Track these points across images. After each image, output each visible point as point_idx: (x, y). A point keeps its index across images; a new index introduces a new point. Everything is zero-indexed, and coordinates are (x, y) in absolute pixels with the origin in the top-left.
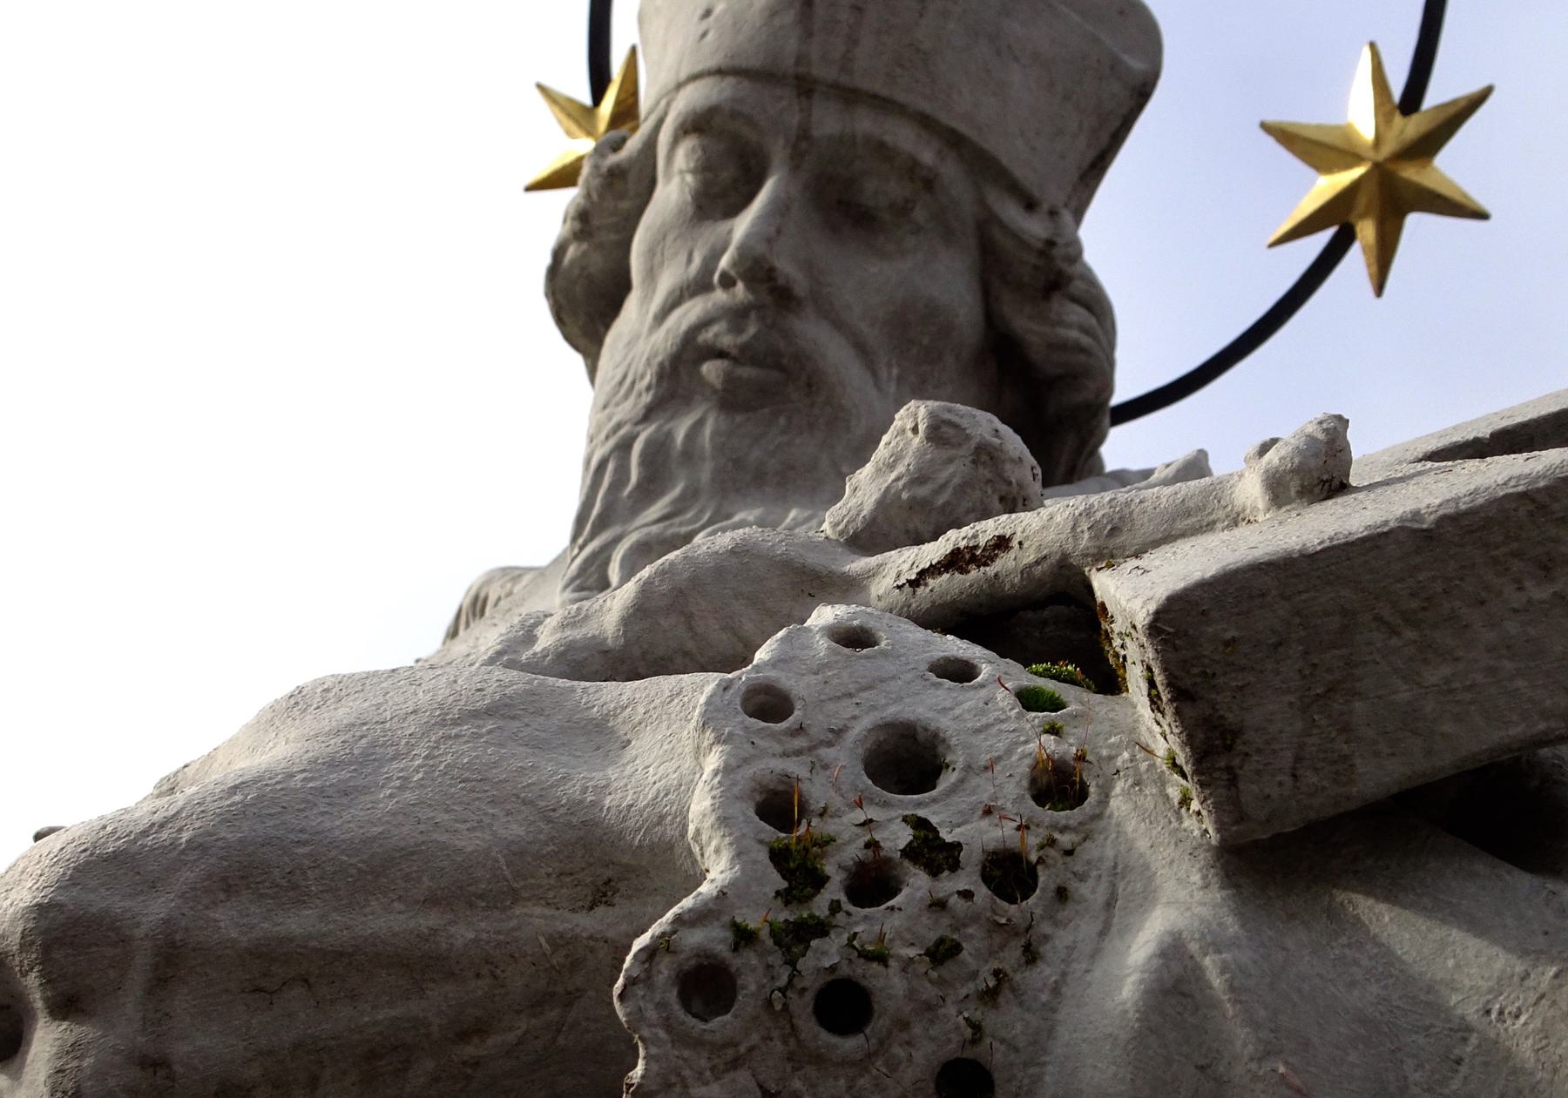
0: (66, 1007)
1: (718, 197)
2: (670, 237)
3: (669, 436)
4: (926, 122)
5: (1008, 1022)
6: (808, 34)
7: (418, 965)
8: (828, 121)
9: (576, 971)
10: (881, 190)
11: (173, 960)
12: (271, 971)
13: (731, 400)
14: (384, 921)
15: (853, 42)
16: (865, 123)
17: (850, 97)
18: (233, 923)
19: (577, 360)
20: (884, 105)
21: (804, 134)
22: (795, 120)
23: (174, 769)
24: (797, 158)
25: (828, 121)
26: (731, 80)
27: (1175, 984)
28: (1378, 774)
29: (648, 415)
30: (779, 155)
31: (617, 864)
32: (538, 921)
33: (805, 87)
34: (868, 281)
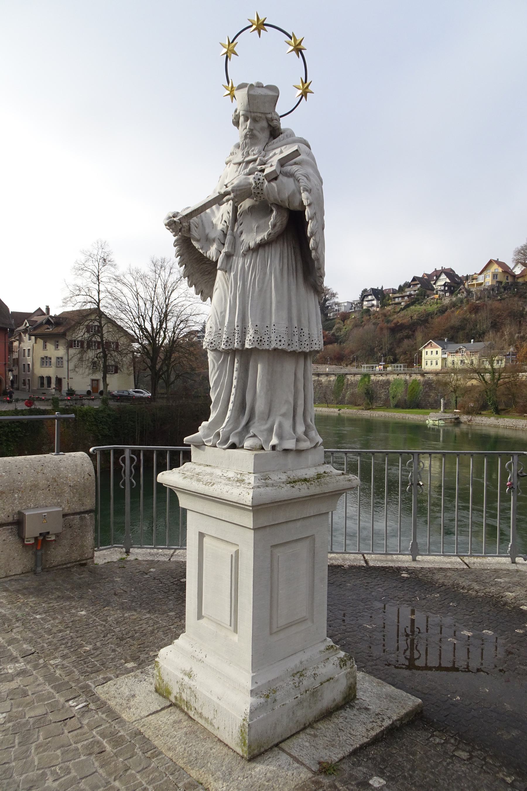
0: (233, 192)
1: (246, 120)
4: (260, 113)
7: (245, 189)
8: (253, 115)
9: (250, 188)
10: (258, 119)
11: (236, 190)
12: (240, 190)
13: (250, 138)
14: (243, 187)
16: (256, 114)
17: (254, 112)
18: (238, 189)
19: (236, 128)
20: (256, 112)
23: (430, 271)
24: (251, 118)
25: (253, 115)
28: (271, 179)
31: (251, 184)
32: (248, 186)
33: (250, 112)
34: (258, 126)
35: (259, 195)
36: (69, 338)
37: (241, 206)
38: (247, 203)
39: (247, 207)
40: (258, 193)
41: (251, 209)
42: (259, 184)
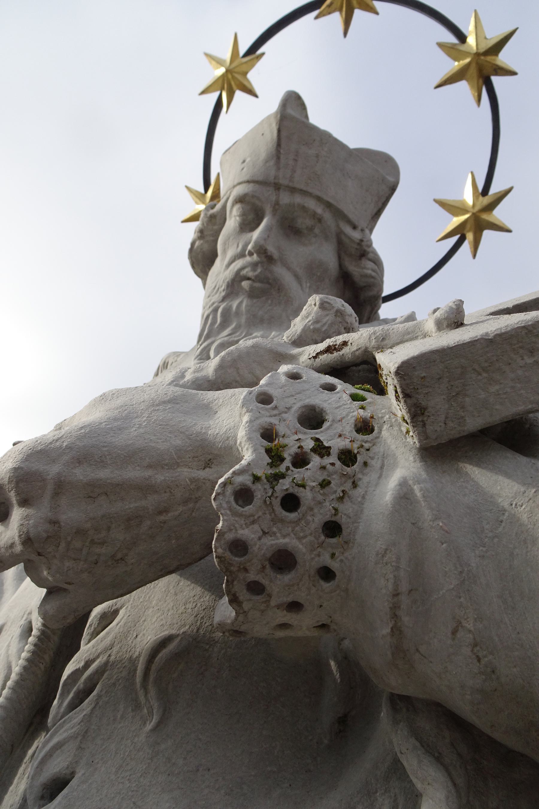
0: (24, 503)
1: (248, 224)
2: (231, 239)
3: (231, 307)
4: (319, 199)
5: (346, 508)
6: (278, 169)
7: (145, 489)
8: (285, 199)
9: (198, 491)
10: (303, 222)
11: (60, 487)
12: (94, 491)
13: (252, 294)
14: (133, 474)
15: (294, 171)
16: (298, 199)
17: (293, 190)
18: (80, 474)
19: (199, 281)
20: (304, 193)
21: (277, 203)
22: (274, 198)
24: (275, 211)
25: (285, 199)
26: (252, 185)
27: (404, 496)
28: (473, 423)
29: (224, 299)
30: (268, 210)
31: (212, 454)
32: (186, 473)
33: (277, 187)
34: (299, 253)
35: (279, 585)
36: (275, 496)
37: (107, 619)
38: (152, 612)
39: (148, 635)
40: (283, 561)
41: (176, 663)
42: (303, 474)
